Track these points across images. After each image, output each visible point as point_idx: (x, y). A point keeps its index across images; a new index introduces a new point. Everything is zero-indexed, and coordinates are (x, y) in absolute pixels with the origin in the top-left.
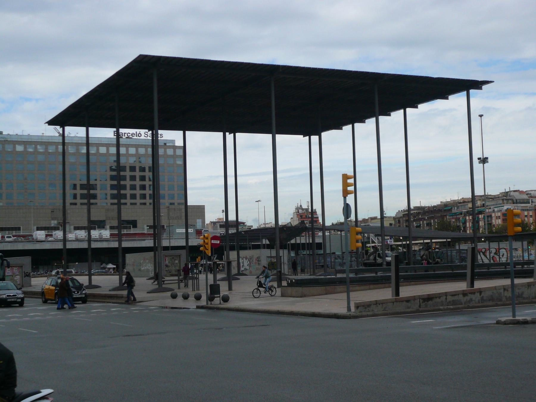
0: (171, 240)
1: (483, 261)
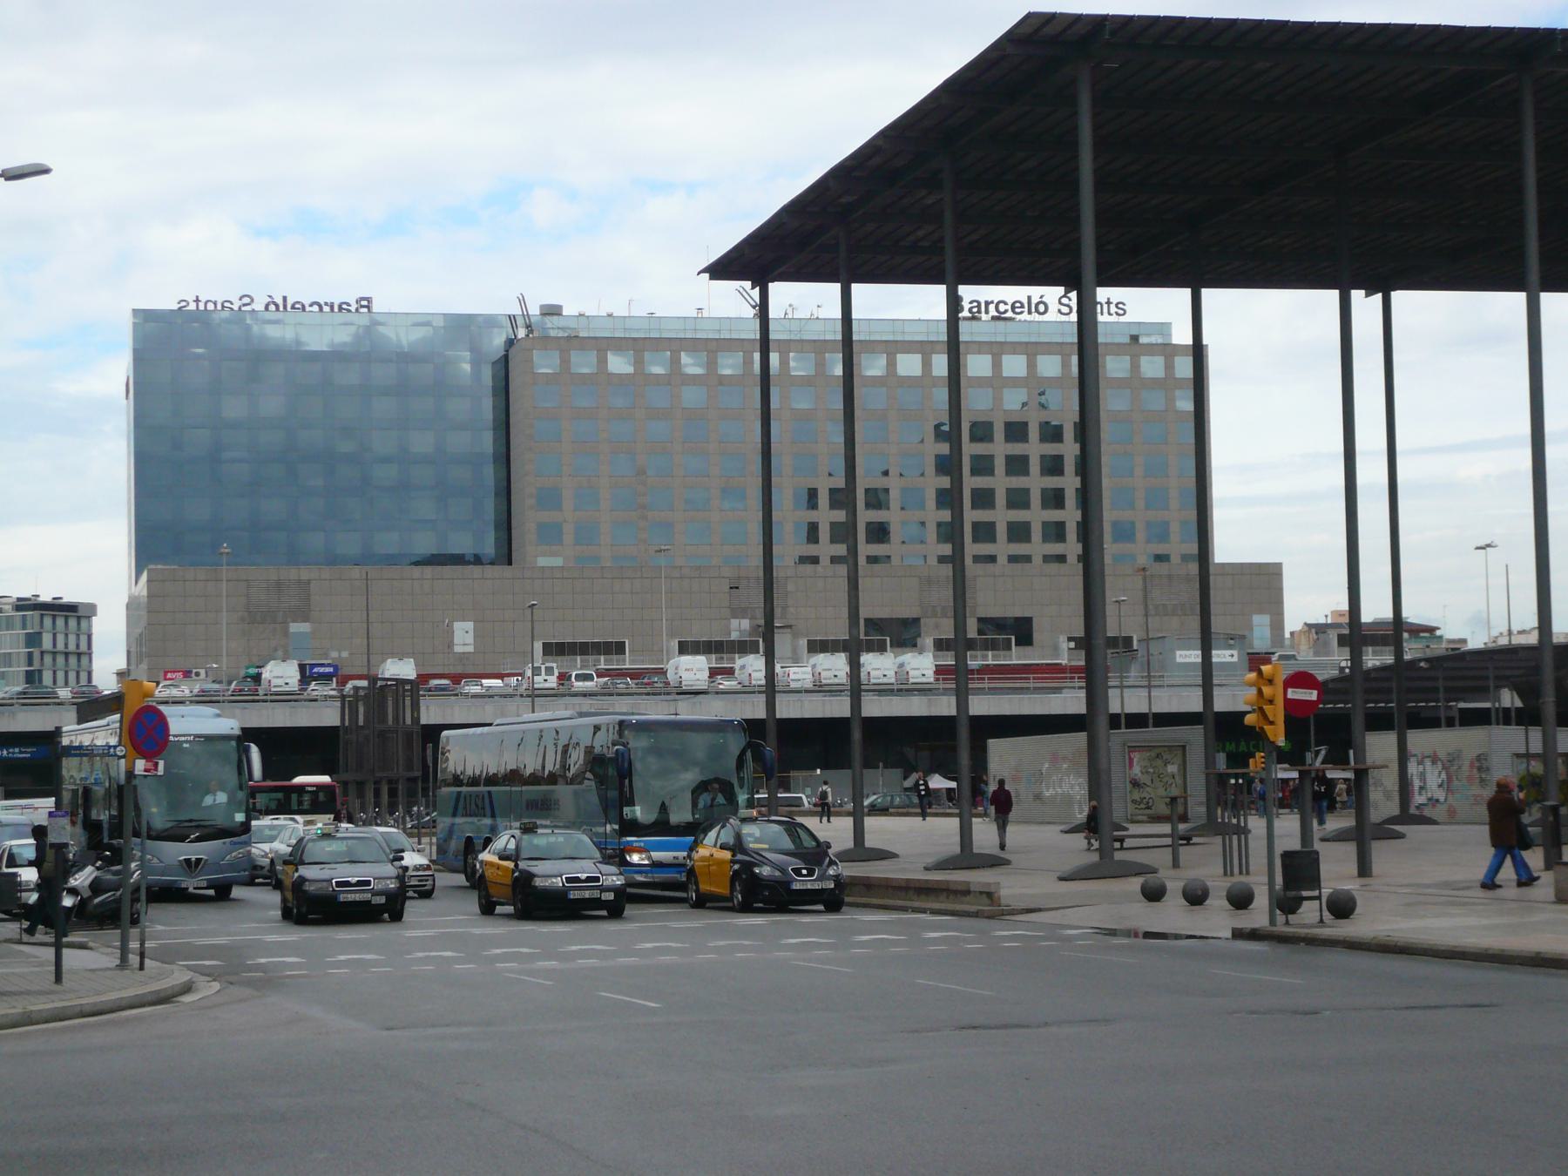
0: (1154, 693)
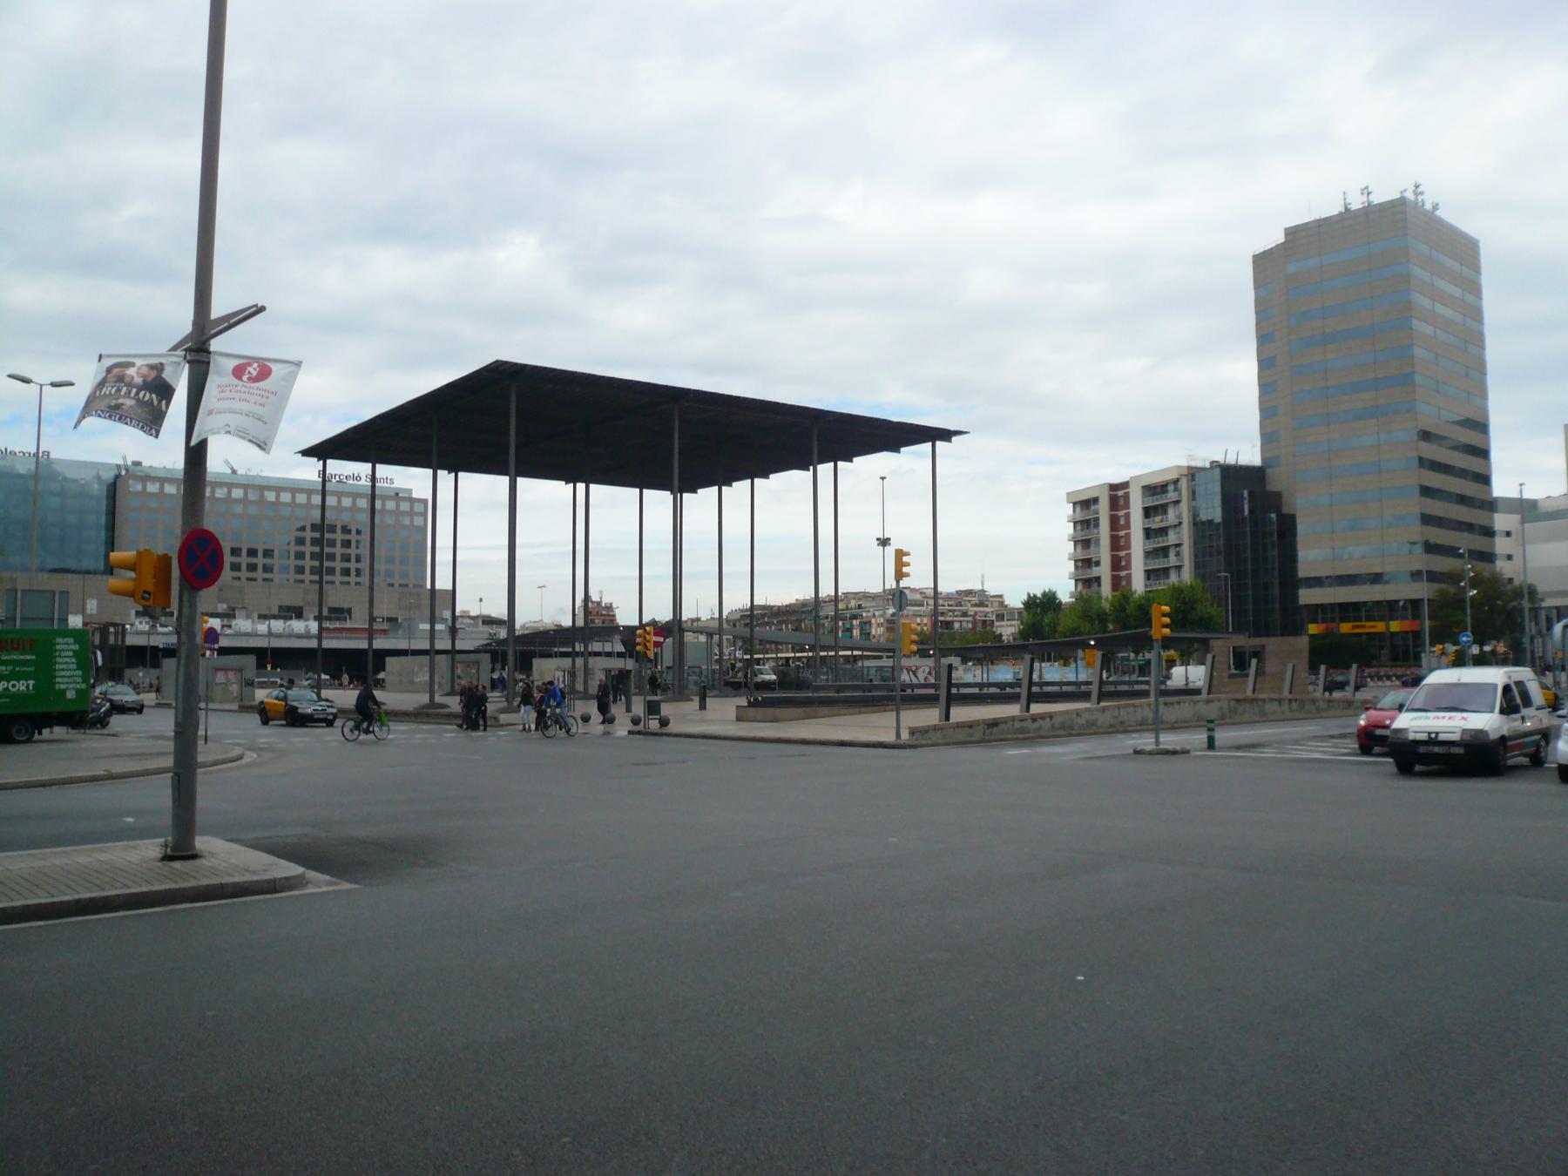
1: (205, 765)
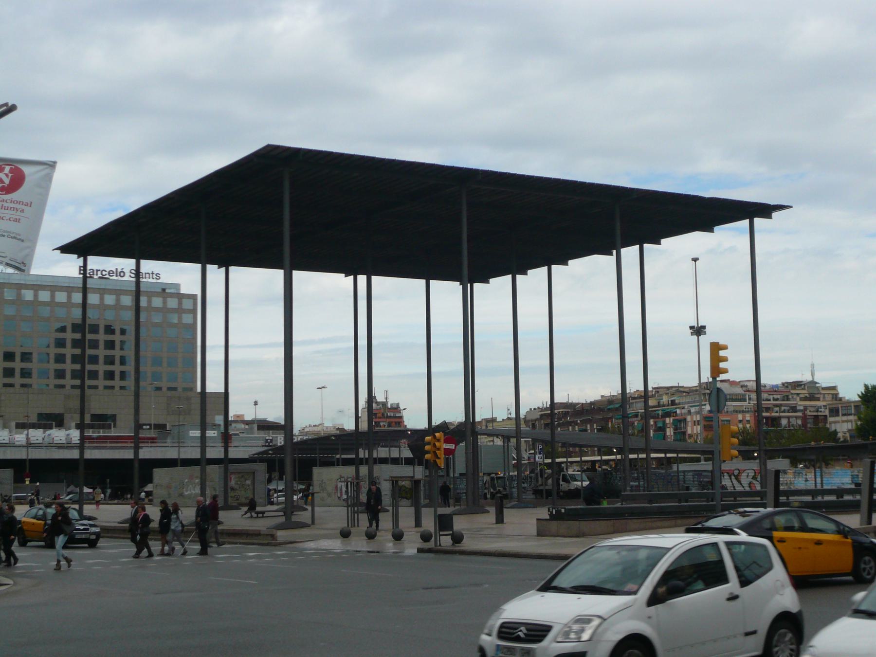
0: (182, 449)
